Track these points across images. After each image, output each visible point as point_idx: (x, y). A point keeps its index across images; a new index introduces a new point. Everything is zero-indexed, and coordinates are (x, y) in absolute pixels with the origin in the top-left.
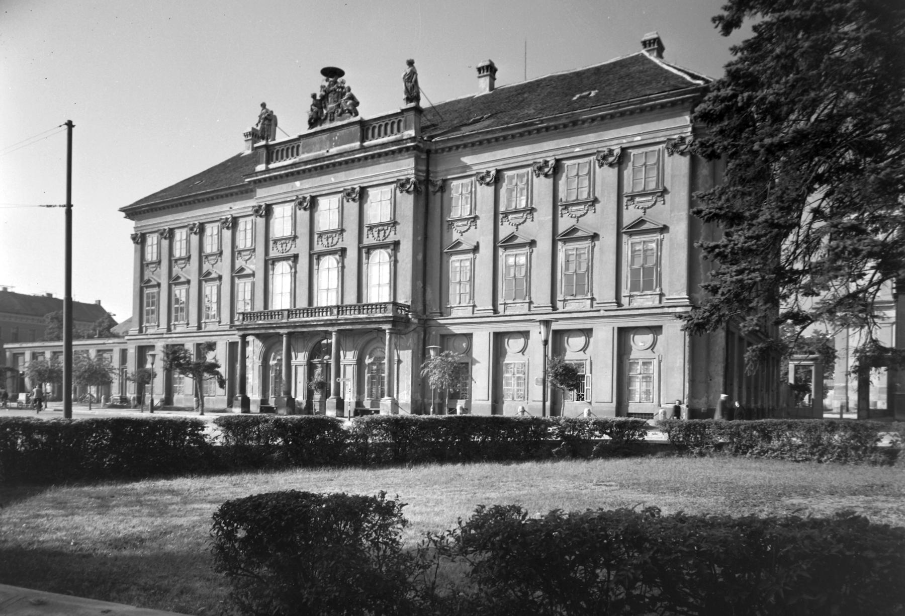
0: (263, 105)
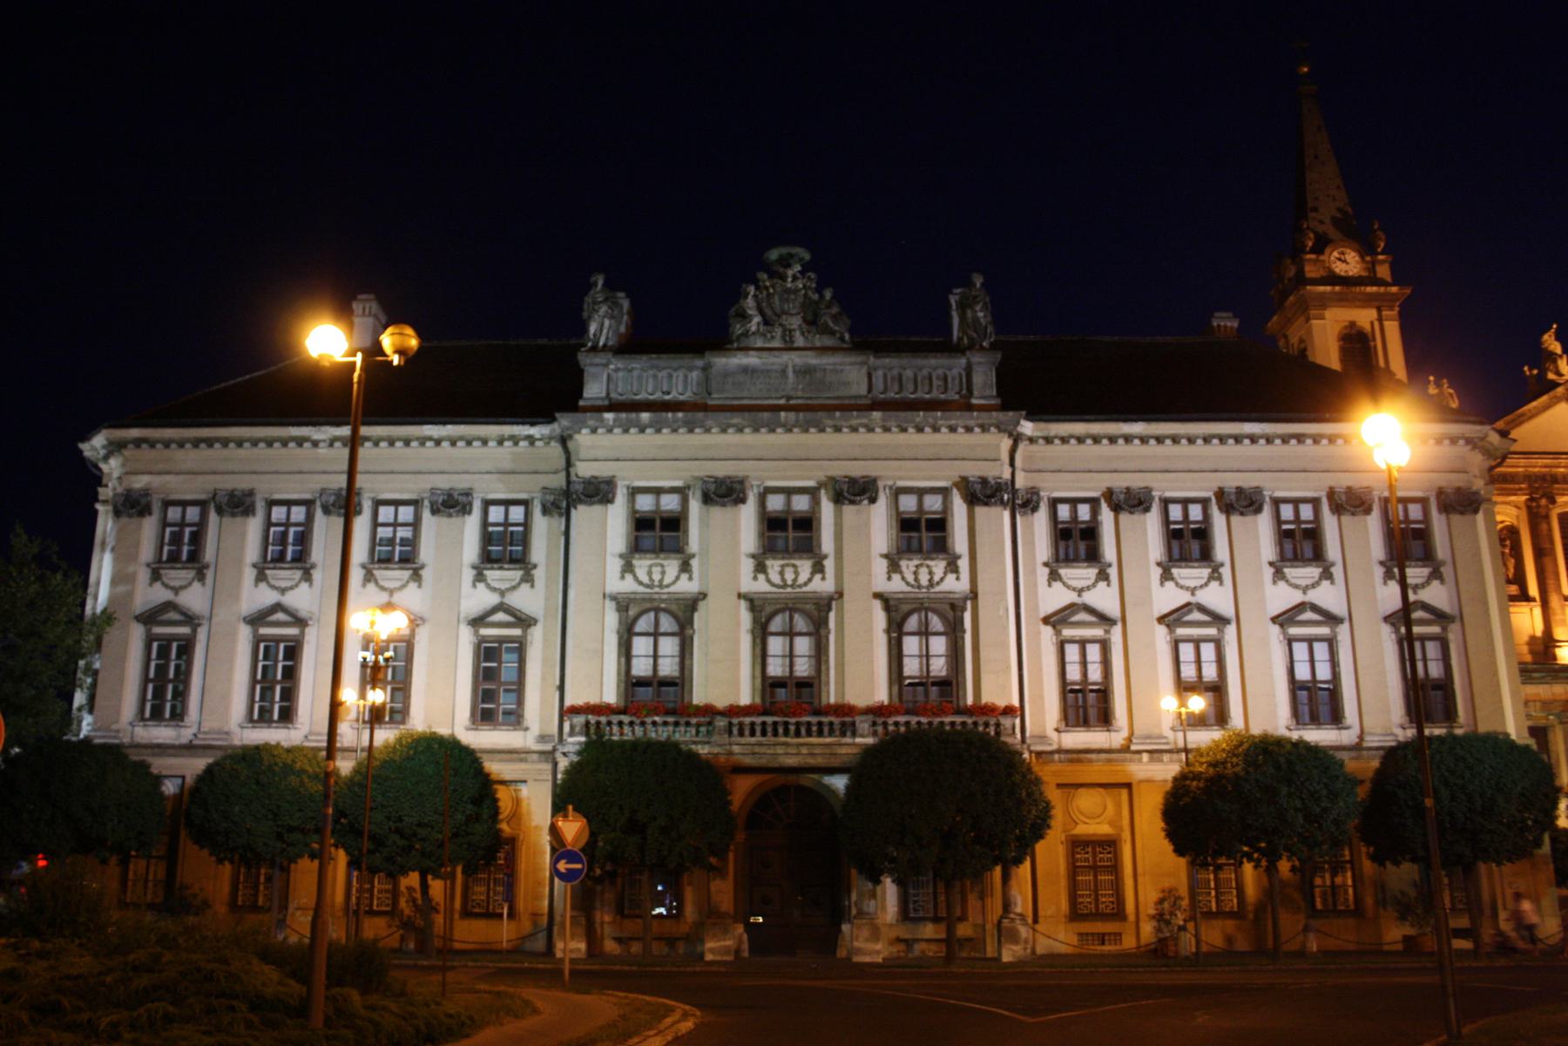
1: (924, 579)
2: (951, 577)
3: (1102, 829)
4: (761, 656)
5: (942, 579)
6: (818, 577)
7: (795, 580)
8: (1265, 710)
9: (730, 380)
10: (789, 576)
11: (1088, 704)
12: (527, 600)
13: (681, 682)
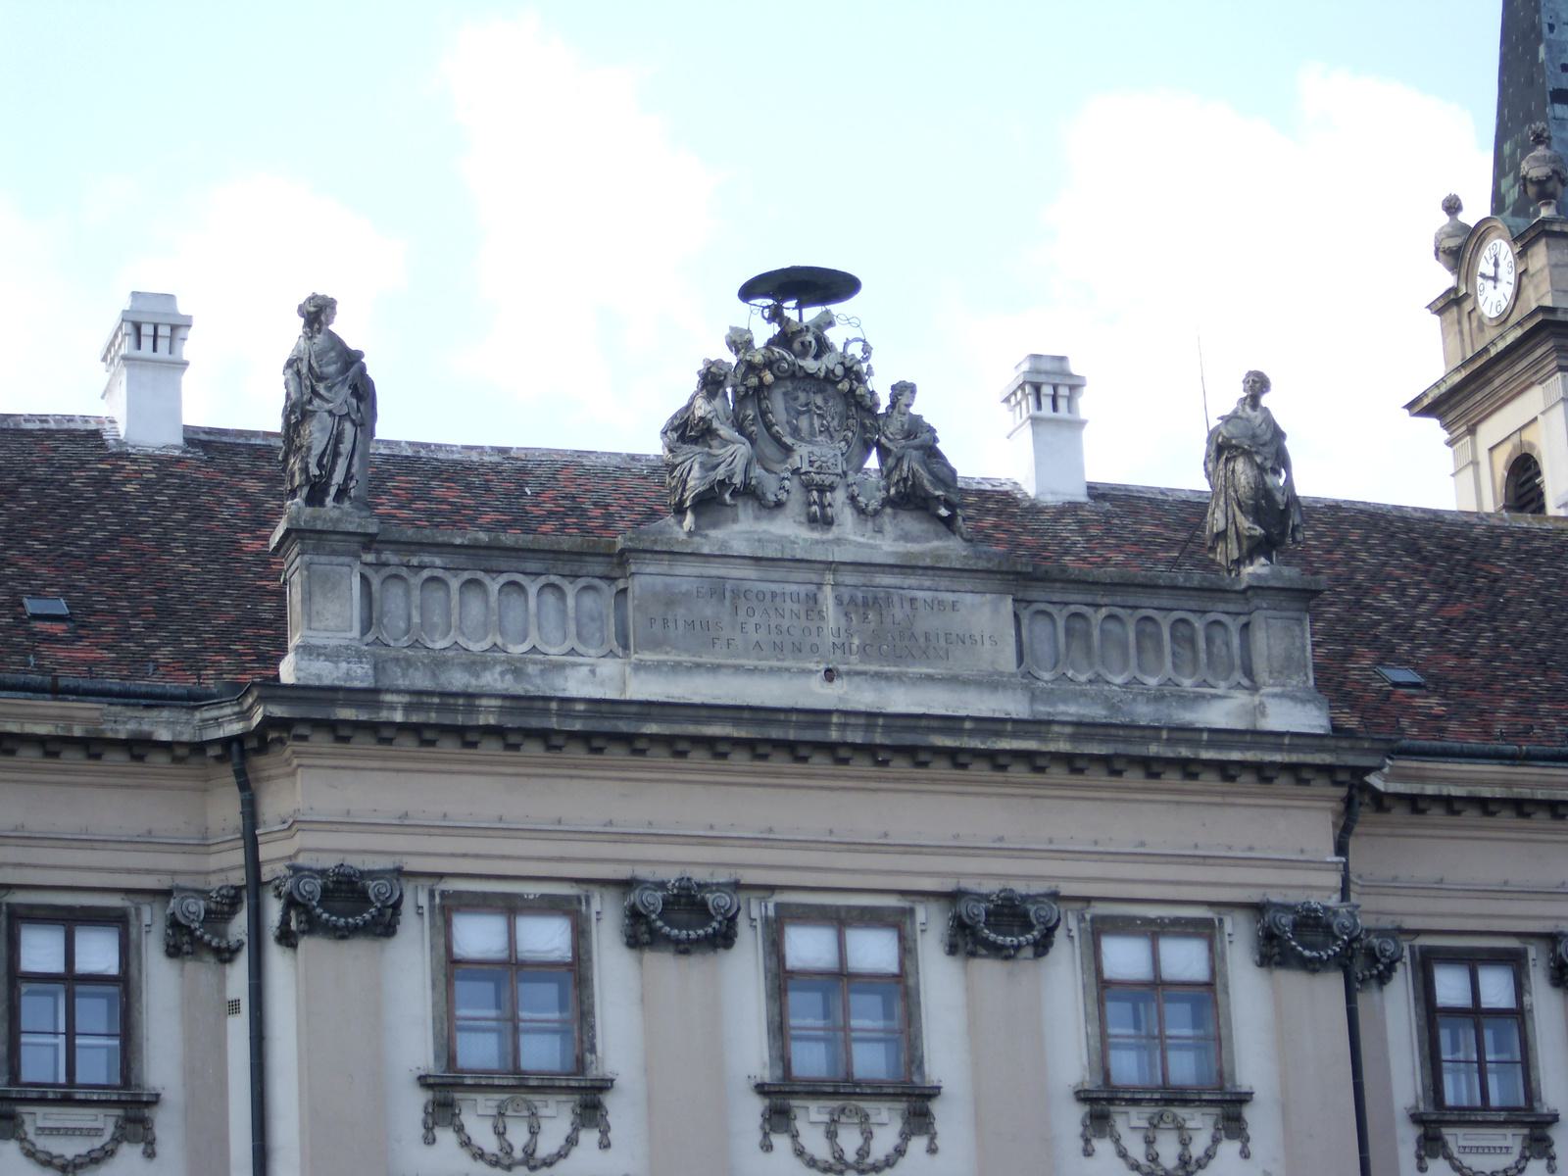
0: (1258, 385)
1: (1168, 1151)
5: (1209, 1155)
6: (918, 1144)
7: (863, 1153)
9: (681, 612)
10: (518, 1135)
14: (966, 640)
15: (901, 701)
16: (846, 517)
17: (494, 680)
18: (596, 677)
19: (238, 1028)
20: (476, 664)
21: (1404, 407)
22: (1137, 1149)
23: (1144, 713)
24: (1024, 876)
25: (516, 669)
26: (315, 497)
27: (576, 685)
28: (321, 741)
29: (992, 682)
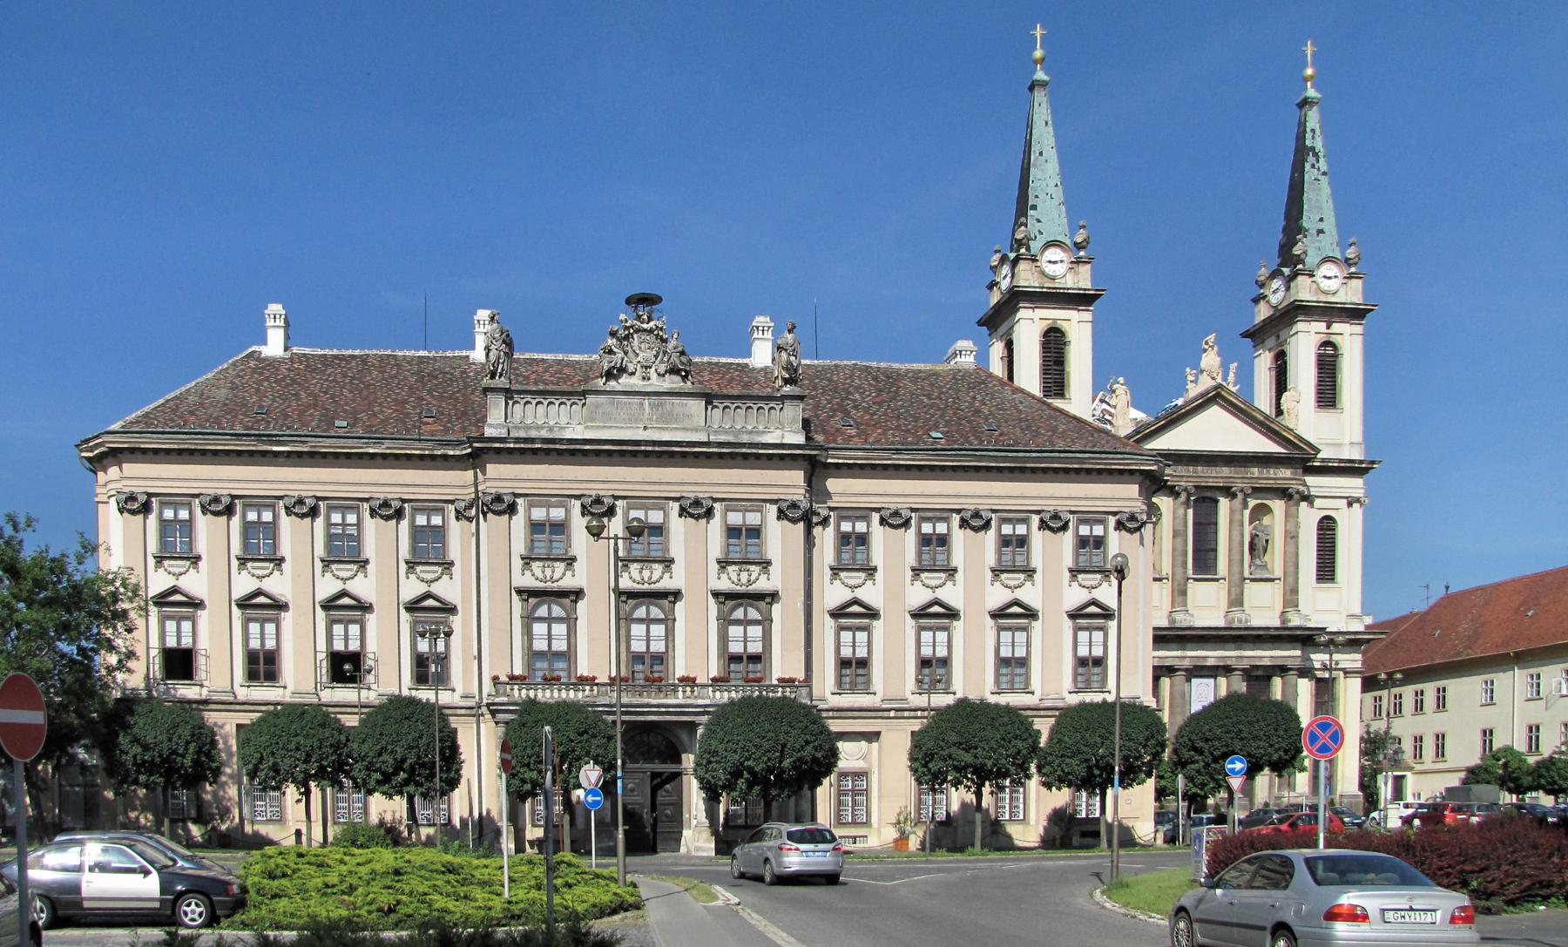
1: (744, 577)
2: (763, 577)
3: (859, 765)
4: (724, 639)
6: (569, 573)
8: (972, 680)
11: (854, 669)
12: (448, 589)
13: (569, 656)
14: (689, 416)
15: (666, 437)
16: (654, 375)
17: (544, 434)
18: (578, 432)
19: (474, 539)
20: (539, 428)
21: (980, 323)
22: (735, 578)
23: (745, 439)
24: (702, 493)
25: (551, 429)
26: (493, 377)
27: (568, 435)
28: (492, 455)
29: (696, 430)
